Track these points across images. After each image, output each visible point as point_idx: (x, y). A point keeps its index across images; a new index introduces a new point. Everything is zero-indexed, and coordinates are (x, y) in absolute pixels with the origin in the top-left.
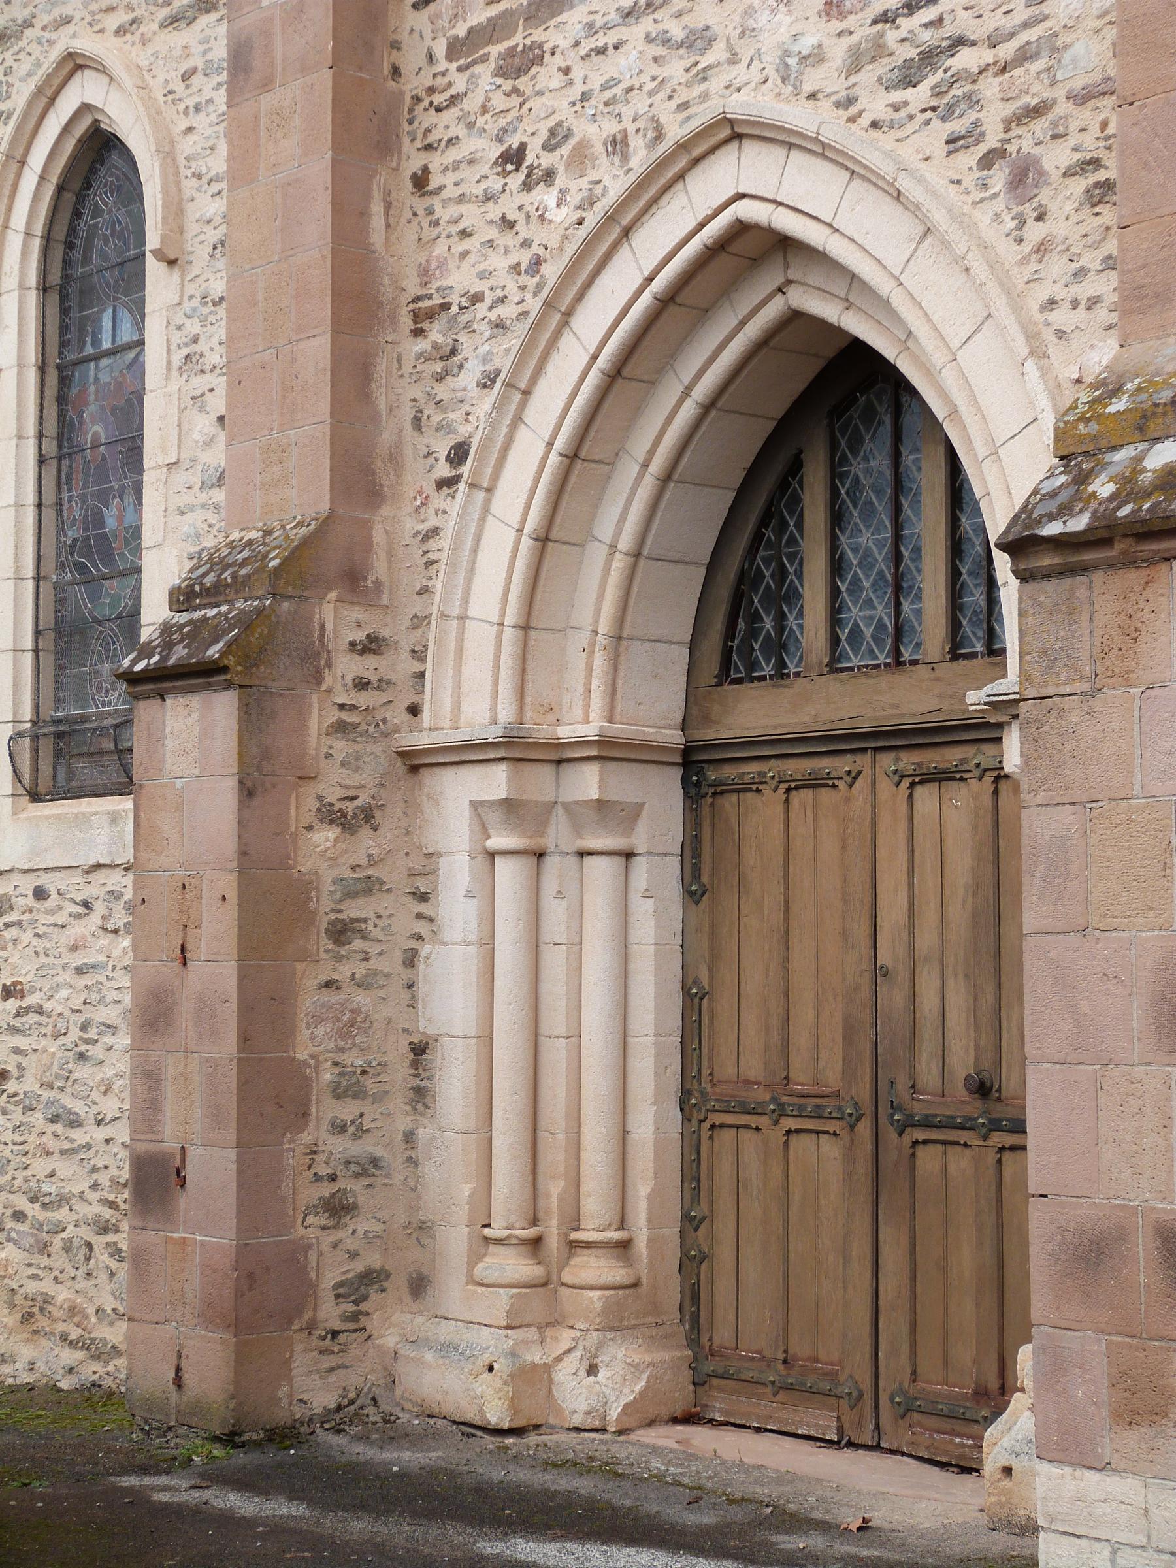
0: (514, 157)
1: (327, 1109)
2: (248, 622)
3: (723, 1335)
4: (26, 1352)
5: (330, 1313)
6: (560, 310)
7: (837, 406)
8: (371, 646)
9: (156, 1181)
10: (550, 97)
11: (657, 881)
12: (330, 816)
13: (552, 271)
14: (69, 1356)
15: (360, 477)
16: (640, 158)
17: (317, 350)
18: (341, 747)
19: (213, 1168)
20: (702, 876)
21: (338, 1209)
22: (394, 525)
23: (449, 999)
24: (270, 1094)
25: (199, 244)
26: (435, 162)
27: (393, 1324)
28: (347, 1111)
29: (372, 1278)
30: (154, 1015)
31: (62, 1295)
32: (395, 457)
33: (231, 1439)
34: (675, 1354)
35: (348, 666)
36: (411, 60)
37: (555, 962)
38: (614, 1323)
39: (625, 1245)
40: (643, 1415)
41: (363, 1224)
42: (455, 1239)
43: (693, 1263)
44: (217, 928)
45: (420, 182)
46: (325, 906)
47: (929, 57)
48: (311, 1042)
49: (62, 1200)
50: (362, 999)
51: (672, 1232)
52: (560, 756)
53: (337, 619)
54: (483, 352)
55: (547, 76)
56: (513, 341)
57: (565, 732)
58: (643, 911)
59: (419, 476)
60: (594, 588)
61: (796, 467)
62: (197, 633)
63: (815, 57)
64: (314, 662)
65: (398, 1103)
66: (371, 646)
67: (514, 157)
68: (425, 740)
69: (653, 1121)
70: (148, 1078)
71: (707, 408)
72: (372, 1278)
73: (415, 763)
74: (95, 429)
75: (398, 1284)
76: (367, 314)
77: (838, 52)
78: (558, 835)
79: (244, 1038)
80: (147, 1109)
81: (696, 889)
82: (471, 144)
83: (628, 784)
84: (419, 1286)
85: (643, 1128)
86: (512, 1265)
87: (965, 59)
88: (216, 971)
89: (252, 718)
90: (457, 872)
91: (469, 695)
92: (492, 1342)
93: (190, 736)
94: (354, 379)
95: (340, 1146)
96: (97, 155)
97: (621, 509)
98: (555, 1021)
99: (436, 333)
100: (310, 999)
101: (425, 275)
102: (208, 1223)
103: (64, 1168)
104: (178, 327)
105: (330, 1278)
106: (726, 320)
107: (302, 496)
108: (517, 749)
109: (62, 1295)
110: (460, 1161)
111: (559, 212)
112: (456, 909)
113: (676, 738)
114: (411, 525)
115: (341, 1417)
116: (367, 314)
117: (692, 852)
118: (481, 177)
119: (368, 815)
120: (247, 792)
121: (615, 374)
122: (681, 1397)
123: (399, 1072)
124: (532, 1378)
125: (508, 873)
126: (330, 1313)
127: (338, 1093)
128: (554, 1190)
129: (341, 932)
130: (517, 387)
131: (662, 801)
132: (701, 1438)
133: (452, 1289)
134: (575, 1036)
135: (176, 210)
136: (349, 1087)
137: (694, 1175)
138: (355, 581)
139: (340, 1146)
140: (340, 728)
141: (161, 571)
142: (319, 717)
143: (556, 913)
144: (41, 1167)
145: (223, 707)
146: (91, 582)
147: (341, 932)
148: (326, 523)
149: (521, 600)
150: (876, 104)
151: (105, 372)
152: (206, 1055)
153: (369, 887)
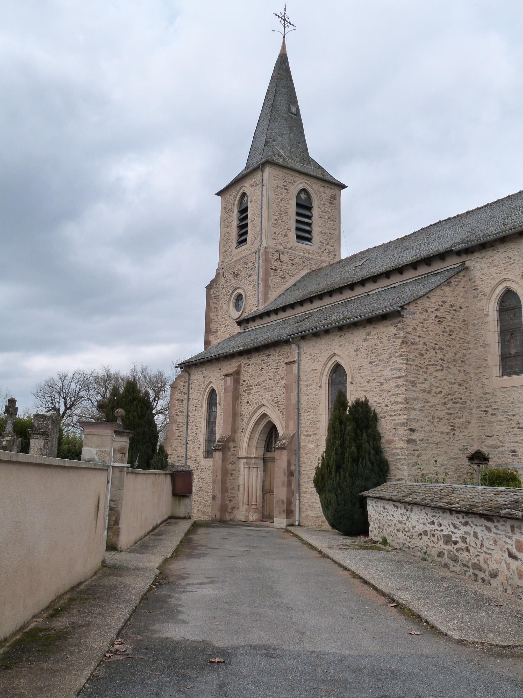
0: (248, 402)
1: (229, 491)
2: (223, 445)
3: (265, 513)
4: (203, 517)
5: (229, 510)
6: (251, 418)
7: (272, 429)
8: (235, 447)
9: (214, 498)
10: (251, 398)
11: (260, 470)
12: (231, 463)
13: (251, 414)
14: (207, 517)
15: (234, 431)
16: (258, 405)
17: (231, 418)
18: (232, 457)
19: (219, 496)
20: (264, 470)
21: (231, 501)
22: (238, 435)
23: (241, 481)
24: (224, 490)
25: (222, 403)
26: (242, 401)
27: (236, 512)
28: (232, 491)
29: (234, 508)
30: (214, 482)
31: (207, 511)
32: (238, 429)
33: (220, 522)
34: (261, 515)
35: (233, 449)
36: (240, 391)
37: (251, 478)
38: (255, 512)
39: (256, 505)
40: (258, 520)
41: (233, 502)
42: (241, 504)
43: (263, 506)
44: (220, 474)
45: (241, 402)
46: (230, 472)
47: (277, 402)
48: (228, 485)
49: (207, 501)
50: (233, 481)
51: (261, 504)
52: (251, 458)
53: (232, 444)
54: (246, 420)
55: (251, 395)
56: (247, 420)
57: (252, 456)
58: (259, 473)
59: (240, 431)
60: (254, 443)
61: (272, 433)
62: (219, 446)
63: (270, 400)
64: (229, 449)
65: (237, 491)
66: (235, 447)
67: (248, 402)
68: (239, 456)
69: (260, 493)
70: (213, 488)
71: (264, 427)
72: (234, 508)
73: (239, 458)
74: (212, 419)
75: (236, 508)
76: (235, 415)
77: (271, 400)
78: (251, 466)
79: (222, 484)
80: (213, 491)
81: (264, 471)
82: (245, 400)
83: (257, 461)
84: (238, 508)
85: (258, 494)
86: (245, 506)
87: (279, 403)
88: (220, 478)
89: (223, 454)
90: (242, 469)
91: (243, 452)
92: (243, 513)
93: (218, 455)
94: (234, 422)
95: (230, 495)
96: (213, 391)
97: (257, 435)
98: (250, 484)
99: (242, 417)
100: (228, 481)
101: (241, 411)
102: (218, 501)
103: (207, 497)
104: (219, 410)
105: (229, 507)
106: (265, 420)
107: (229, 433)
108: (247, 458)
109: (207, 511)
110: (241, 497)
111: (251, 408)
112: (242, 472)
113: (262, 457)
114: (239, 435)
115: (230, 520)
116: (235, 415)
117: (264, 467)
118: (245, 403)
119: (234, 463)
120: (223, 461)
121: (256, 424)
122: (261, 518)
123: (237, 488)
124: (247, 517)
125: (247, 469)
126: (229, 510)
127: (231, 490)
128: (250, 499)
129: (231, 474)
130: (248, 424)
131: (261, 462)
132: (262, 522)
133: (241, 509)
134: (252, 485)
135: (220, 399)
136: (232, 489)
137: (263, 498)
138: (233, 441)
139: (230, 495)
140: (232, 455)
141: (218, 437)
142: (230, 454)
143: (251, 473)
144: (205, 497)
145: (221, 453)
146: (212, 437)
147: (231, 474)
148: (231, 436)
149: (248, 444)
150: (274, 405)
151: (213, 413)
152: (219, 485)
153: (234, 470)
